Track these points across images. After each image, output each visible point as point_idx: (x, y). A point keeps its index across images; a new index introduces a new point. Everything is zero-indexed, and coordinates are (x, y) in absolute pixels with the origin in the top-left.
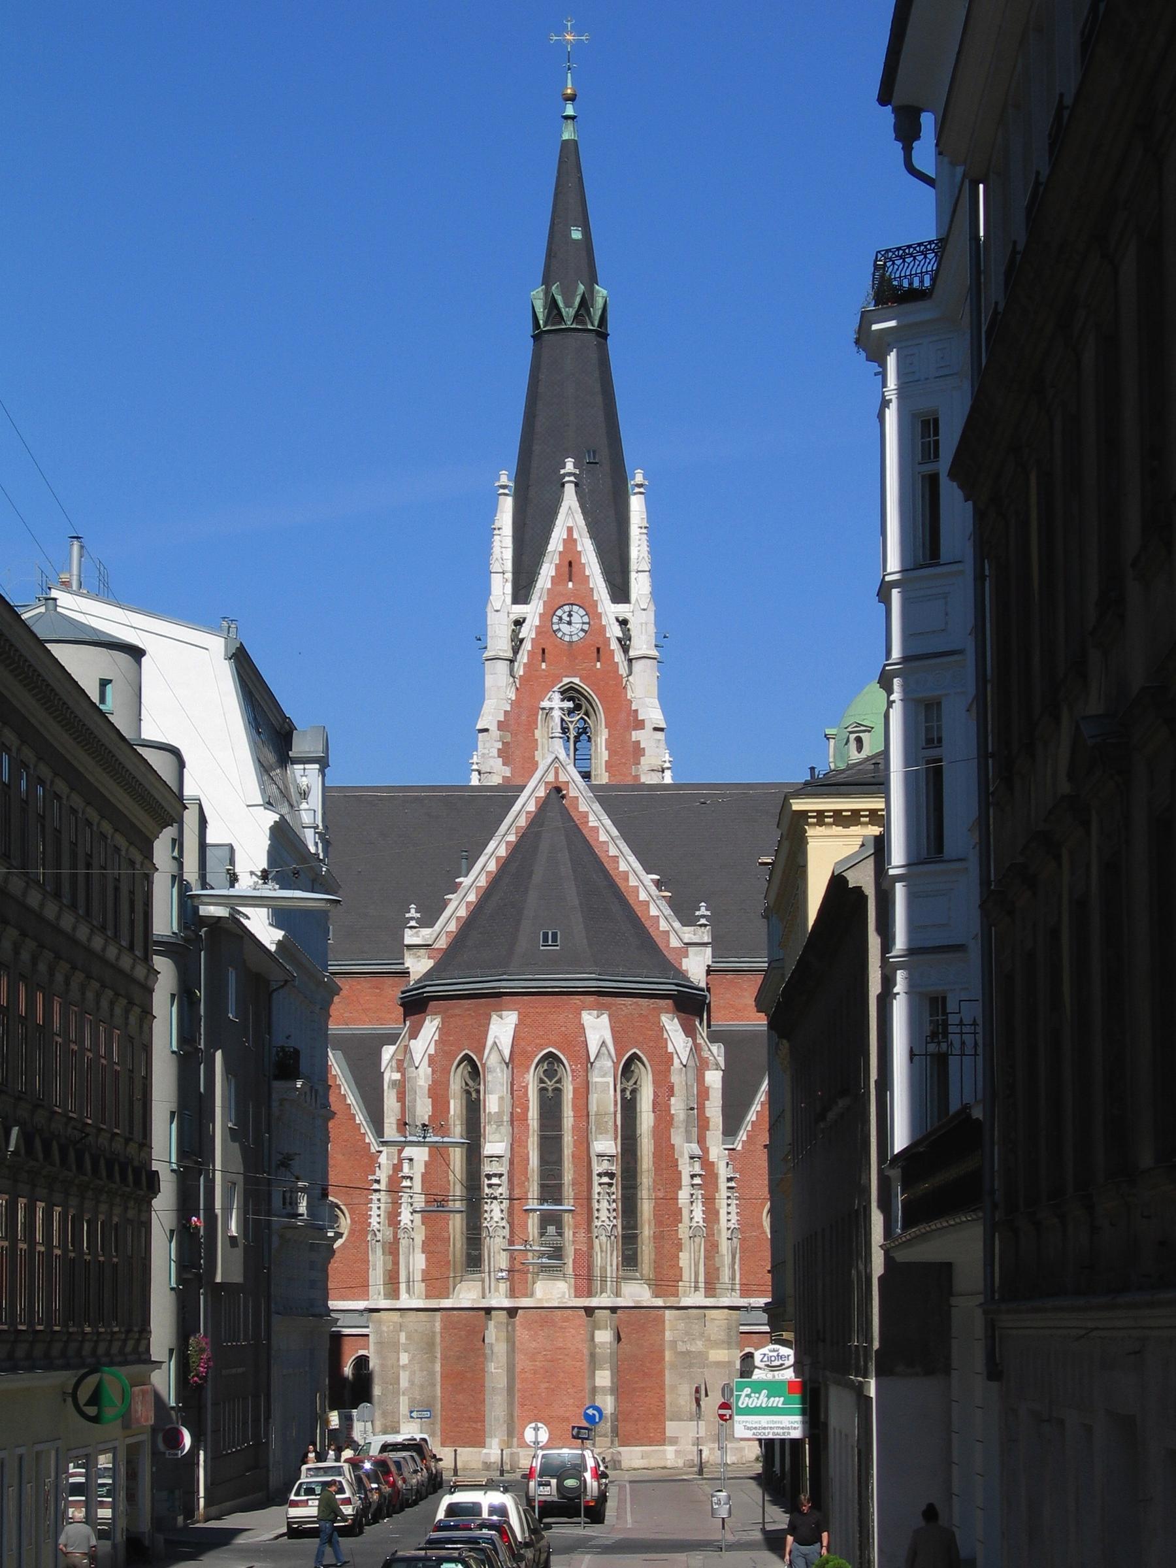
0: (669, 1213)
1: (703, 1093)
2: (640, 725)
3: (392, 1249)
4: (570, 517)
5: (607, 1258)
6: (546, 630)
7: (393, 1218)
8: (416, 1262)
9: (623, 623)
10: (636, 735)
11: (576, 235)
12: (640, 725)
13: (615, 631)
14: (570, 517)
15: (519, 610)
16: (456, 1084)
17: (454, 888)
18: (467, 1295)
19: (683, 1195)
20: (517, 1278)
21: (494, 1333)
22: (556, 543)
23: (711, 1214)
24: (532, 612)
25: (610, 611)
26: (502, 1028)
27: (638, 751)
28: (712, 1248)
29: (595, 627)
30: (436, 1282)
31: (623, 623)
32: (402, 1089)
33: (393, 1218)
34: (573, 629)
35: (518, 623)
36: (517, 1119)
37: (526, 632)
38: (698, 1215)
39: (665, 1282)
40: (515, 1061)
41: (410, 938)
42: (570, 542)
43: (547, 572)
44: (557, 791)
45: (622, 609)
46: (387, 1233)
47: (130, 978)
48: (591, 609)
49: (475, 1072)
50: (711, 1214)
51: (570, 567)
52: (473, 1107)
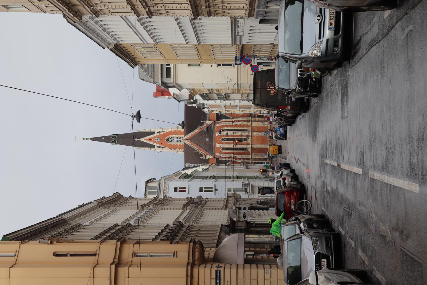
0: (241, 126)
1: (226, 122)
2: (171, 130)
3: (244, 159)
4: (142, 140)
5: (246, 133)
6: (158, 143)
7: (240, 159)
8: (245, 156)
9: (157, 133)
10: (173, 131)
11: (103, 138)
12: (171, 130)
13: (159, 134)
14: (142, 140)
15: (156, 147)
16: (224, 151)
17: (198, 152)
18: (250, 150)
19: (238, 124)
20: (248, 144)
21: (254, 147)
22: (147, 142)
23: (241, 121)
24: (156, 145)
25: (156, 134)
26: (218, 145)
27: (175, 131)
28: (244, 121)
29: (158, 136)
30: (248, 154)
31: (157, 133)
32: (225, 158)
33: (240, 159)
34: (157, 140)
35: (157, 147)
36: (229, 144)
37: (159, 146)
38: (241, 122)
39: (248, 126)
40: (222, 143)
41: (204, 158)
42: (146, 140)
43: (150, 143)
44: (187, 140)
45: (156, 133)
46: (242, 160)
47: (174, 239)
48: (156, 137)
49: (223, 149)
50: (241, 121)
51: (150, 140)
52: (228, 149)
